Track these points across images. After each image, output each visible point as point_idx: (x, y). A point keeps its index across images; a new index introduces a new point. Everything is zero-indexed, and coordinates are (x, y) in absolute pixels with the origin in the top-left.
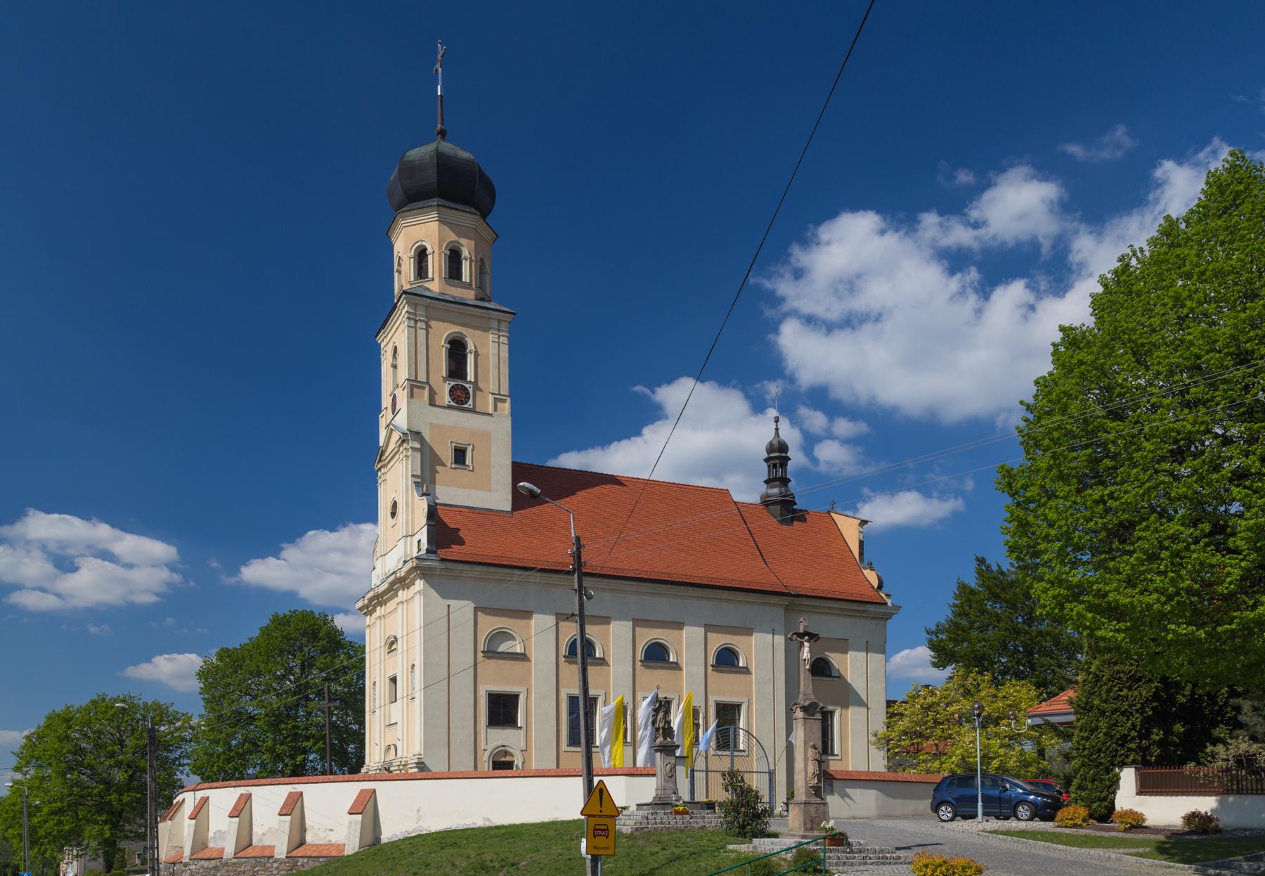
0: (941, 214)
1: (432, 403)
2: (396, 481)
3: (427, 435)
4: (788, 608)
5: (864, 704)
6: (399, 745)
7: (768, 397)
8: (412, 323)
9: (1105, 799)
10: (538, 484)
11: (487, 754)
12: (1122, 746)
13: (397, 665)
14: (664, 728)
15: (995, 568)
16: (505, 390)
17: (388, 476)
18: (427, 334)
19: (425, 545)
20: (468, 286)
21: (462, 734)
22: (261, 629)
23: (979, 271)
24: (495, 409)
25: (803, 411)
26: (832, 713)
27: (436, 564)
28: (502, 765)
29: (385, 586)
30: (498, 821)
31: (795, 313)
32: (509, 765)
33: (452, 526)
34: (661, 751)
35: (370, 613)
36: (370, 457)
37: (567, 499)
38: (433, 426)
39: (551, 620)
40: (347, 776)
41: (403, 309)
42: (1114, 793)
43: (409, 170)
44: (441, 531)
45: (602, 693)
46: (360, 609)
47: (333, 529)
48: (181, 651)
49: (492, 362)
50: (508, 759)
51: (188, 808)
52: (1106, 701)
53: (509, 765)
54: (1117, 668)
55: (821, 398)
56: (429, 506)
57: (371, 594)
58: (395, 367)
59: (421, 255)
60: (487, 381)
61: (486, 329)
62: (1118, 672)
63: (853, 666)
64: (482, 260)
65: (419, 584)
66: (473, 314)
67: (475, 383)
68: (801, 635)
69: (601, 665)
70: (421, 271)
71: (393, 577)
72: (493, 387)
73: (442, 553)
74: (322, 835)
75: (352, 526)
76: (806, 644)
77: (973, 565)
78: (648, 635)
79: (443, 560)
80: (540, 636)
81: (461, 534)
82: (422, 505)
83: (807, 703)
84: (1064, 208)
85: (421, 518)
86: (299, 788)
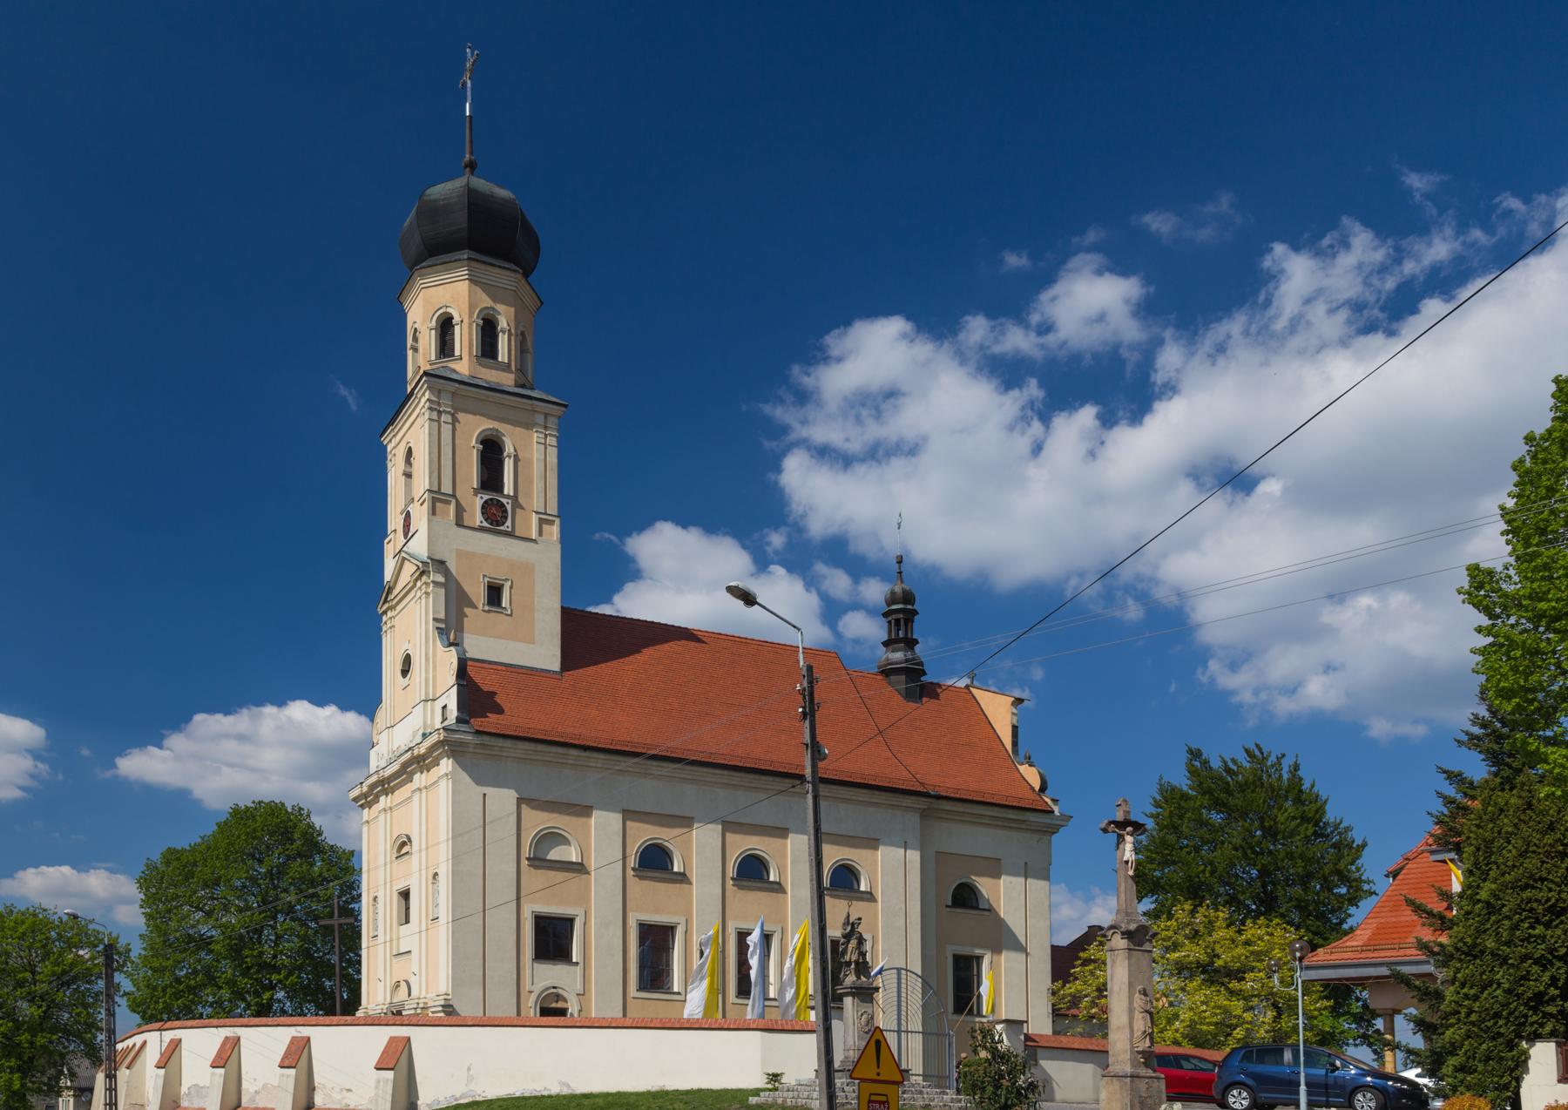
0: (991, 316)
1: (459, 523)
2: (409, 627)
3: (452, 565)
4: (925, 815)
5: (1020, 948)
6: (414, 981)
7: (769, 549)
8: (435, 416)
9: (1506, 1087)
10: (592, 638)
11: (533, 997)
12: (1535, 1009)
13: (413, 874)
14: (857, 963)
15: (1216, 764)
16: (553, 508)
17: (396, 622)
18: (454, 430)
19: (453, 712)
20: (506, 368)
21: (501, 969)
22: (219, 825)
23: (1041, 385)
24: (540, 533)
25: (820, 568)
26: (979, 959)
27: (469, 738)
28: (552, 1011)
29: (395, 767)
30: (581, 1087)
31: (804, 443)
32: (562, 1012)
33: (486, 689)
34: (853, 995)
35: (369, 805)
36: (368, 598)
37: (631, 658)
38: (460, 554)
39: (616, 818)
40: (321, 1019)
41: (423, 398)
42: (1518, 1080)
43: (431, 212)
44: (475, 695)
45: (682, 920)
46: (356, 800)
47: (227, 712)
48: (51, 863)
49: (537, 469)
50: (560, 1005)
51: (152, 1054)
52: (1508, 943)
53: (562, 1012)
54: (1527, 894)
55: (839, 550)
56: (460, 660)
57: (374, 779)
58: (408, 475)
59: (445, 326)
60: (530, 495)
61: (529, 426)
62: (1529, 901)
63: (1007, 895)
64: (523, 333)
65: (446, 765)
66: (516, 402)
67: (515, 498)
68: (1122, 825)
69: (681, 882)
70: (445, 346)
71: (408, 755)
72: (537, 504)
73: (477, 723)
74: (337, 1096)
75: (255, 709)
76: (1129, 839)
77: (1184, 757)
78: (743, 844)
79: (478, 732)
80: (601, 839)
81: (498, 699)
82: (450, 658)
83: (1133, 927)
84: (1146, 310)
85: (448, 675)
86: (305, 1031)
